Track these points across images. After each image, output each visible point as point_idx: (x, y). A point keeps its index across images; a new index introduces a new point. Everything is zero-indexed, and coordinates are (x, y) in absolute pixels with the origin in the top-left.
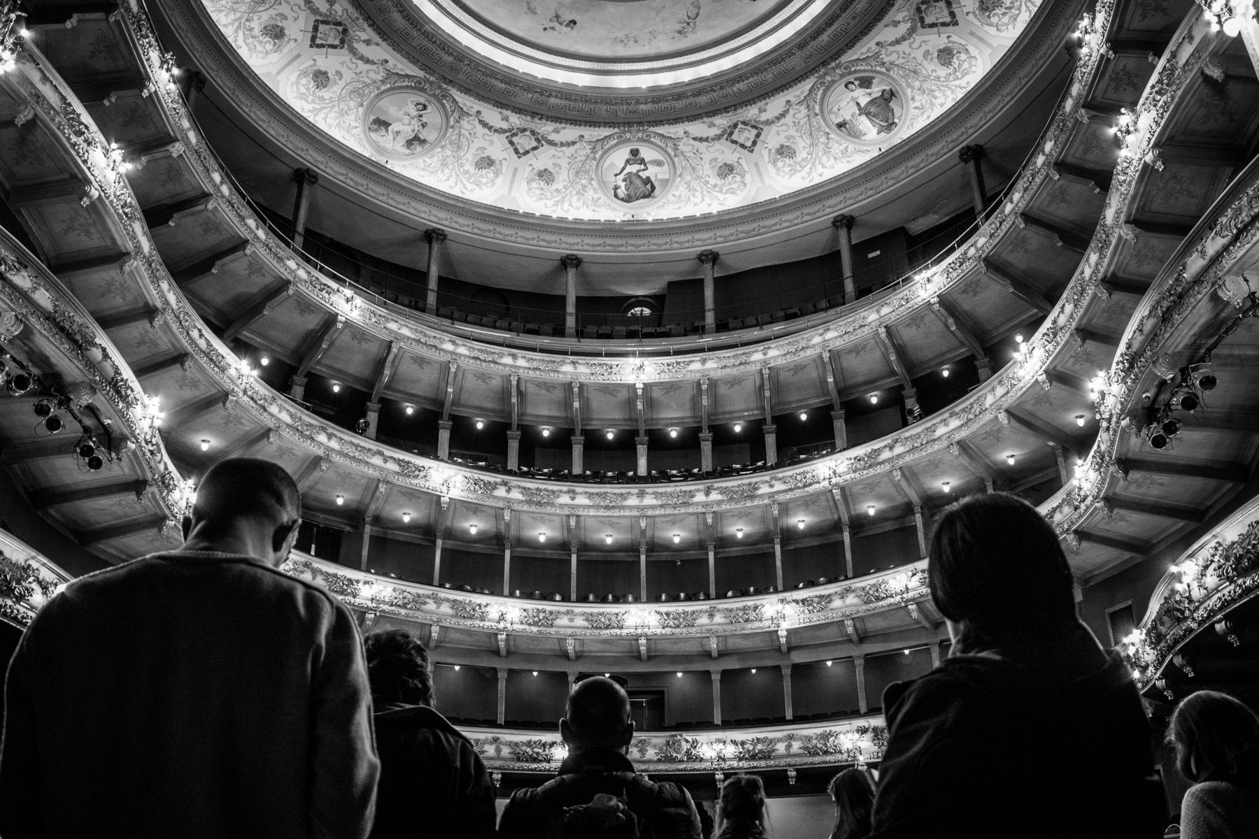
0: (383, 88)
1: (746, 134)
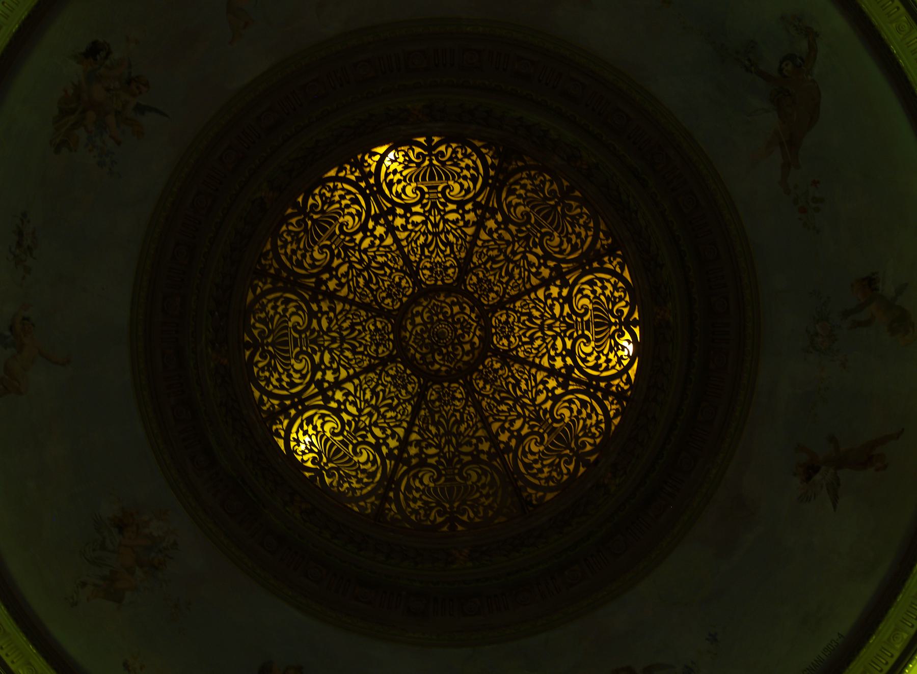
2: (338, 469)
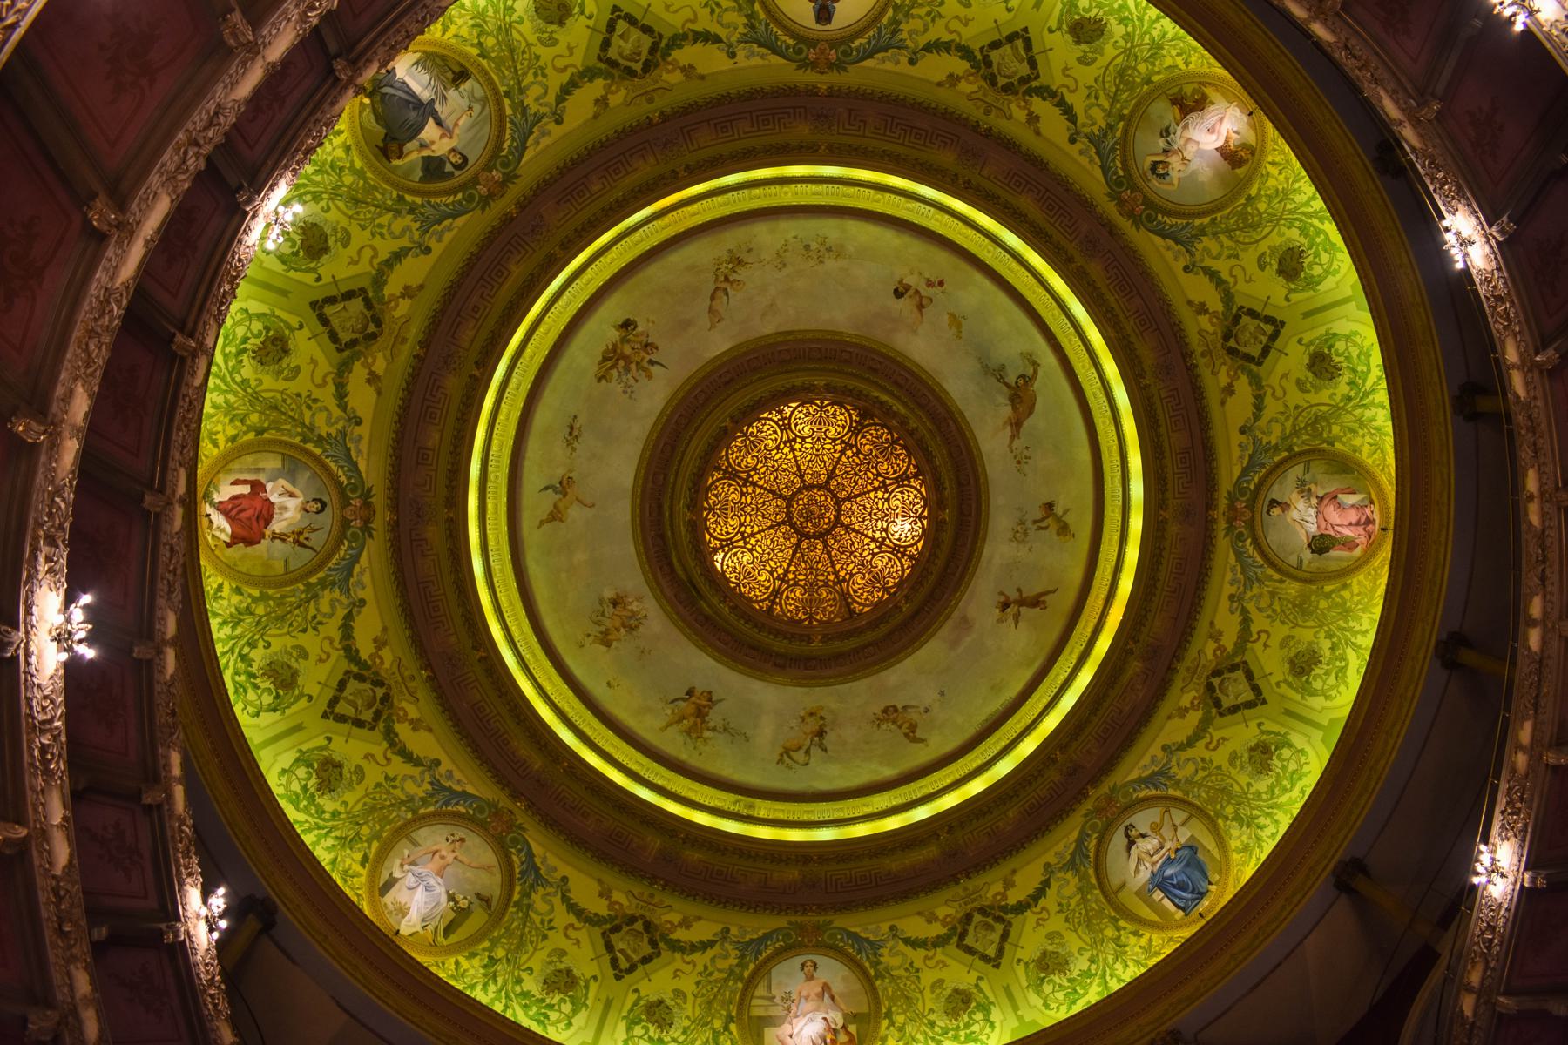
0: (1206, 220)
1: (627, 47)
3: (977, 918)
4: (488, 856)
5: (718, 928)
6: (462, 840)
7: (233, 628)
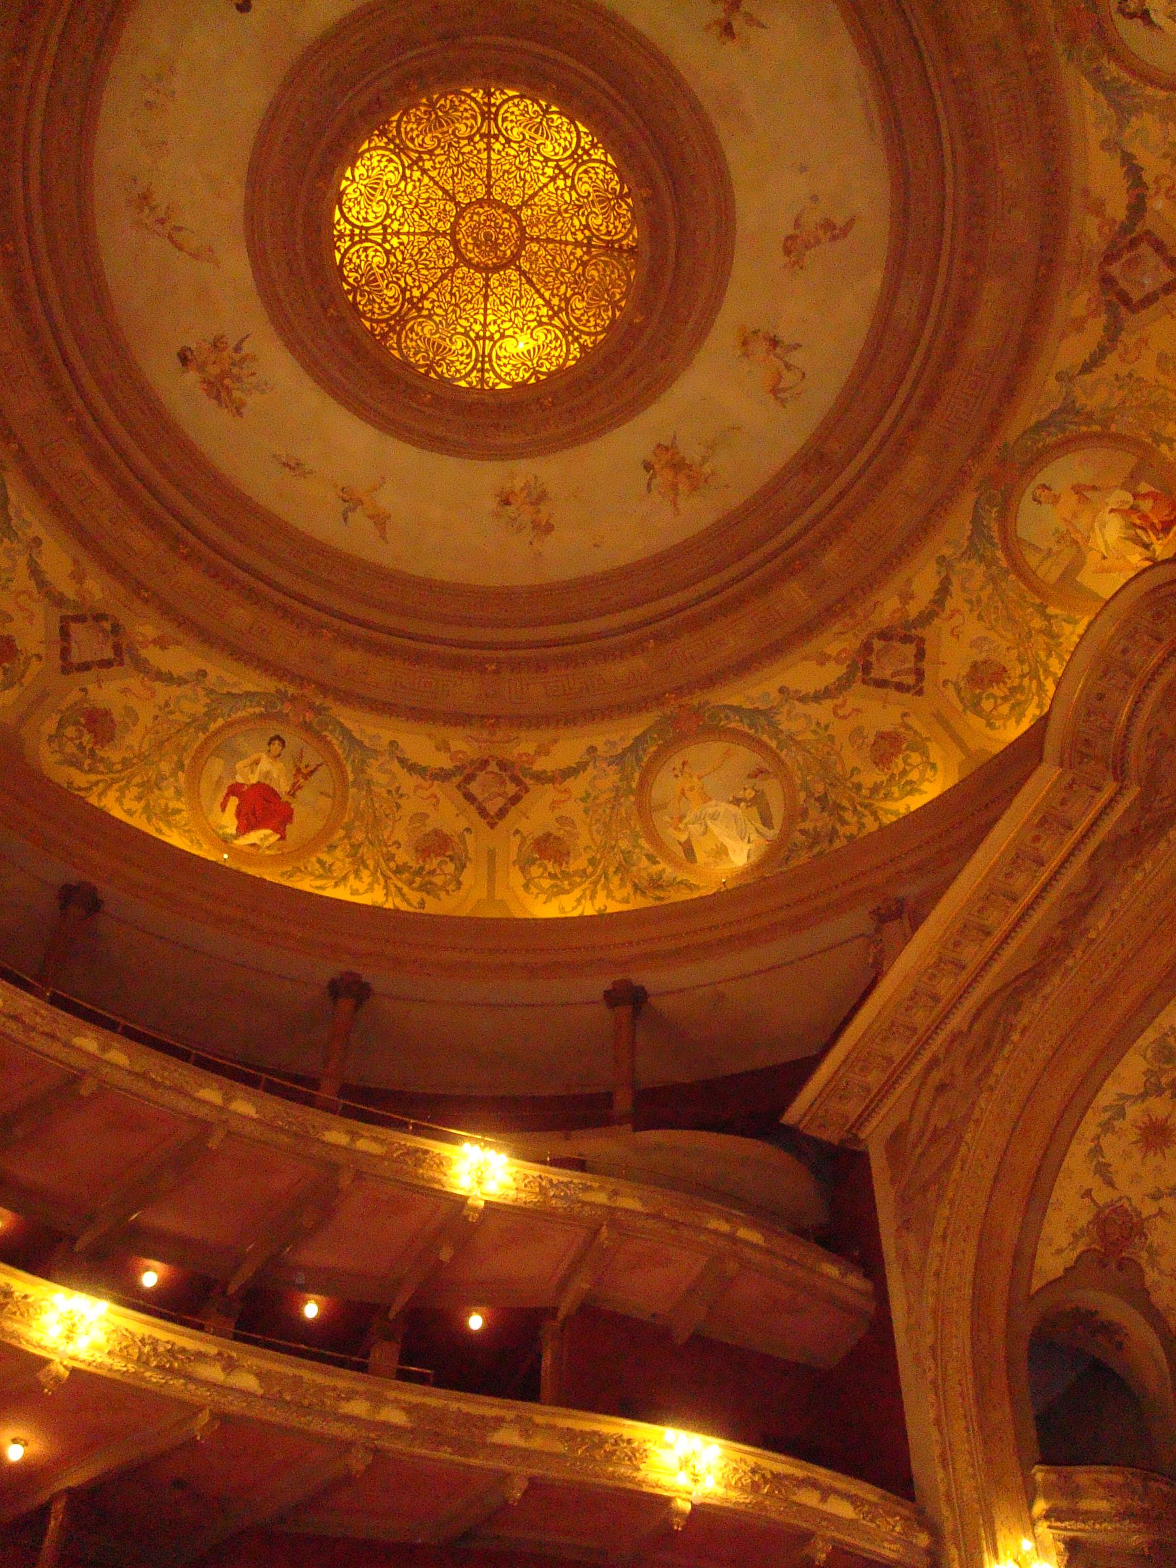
2: (540, 358)
3: (1115, 270)
4: (716, 748)
5: (932, 566)
6: (684, 764)
7: (366, 867)
